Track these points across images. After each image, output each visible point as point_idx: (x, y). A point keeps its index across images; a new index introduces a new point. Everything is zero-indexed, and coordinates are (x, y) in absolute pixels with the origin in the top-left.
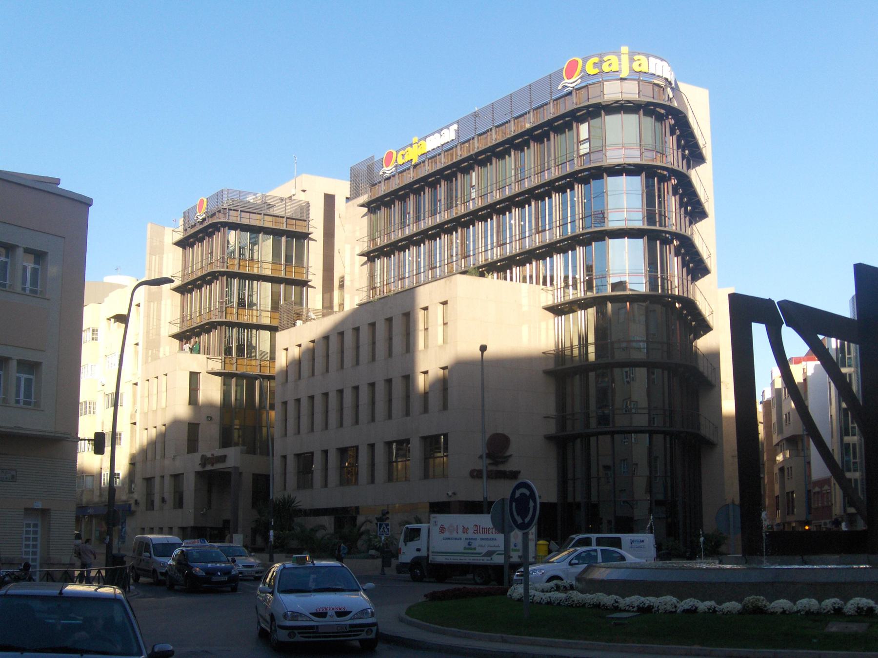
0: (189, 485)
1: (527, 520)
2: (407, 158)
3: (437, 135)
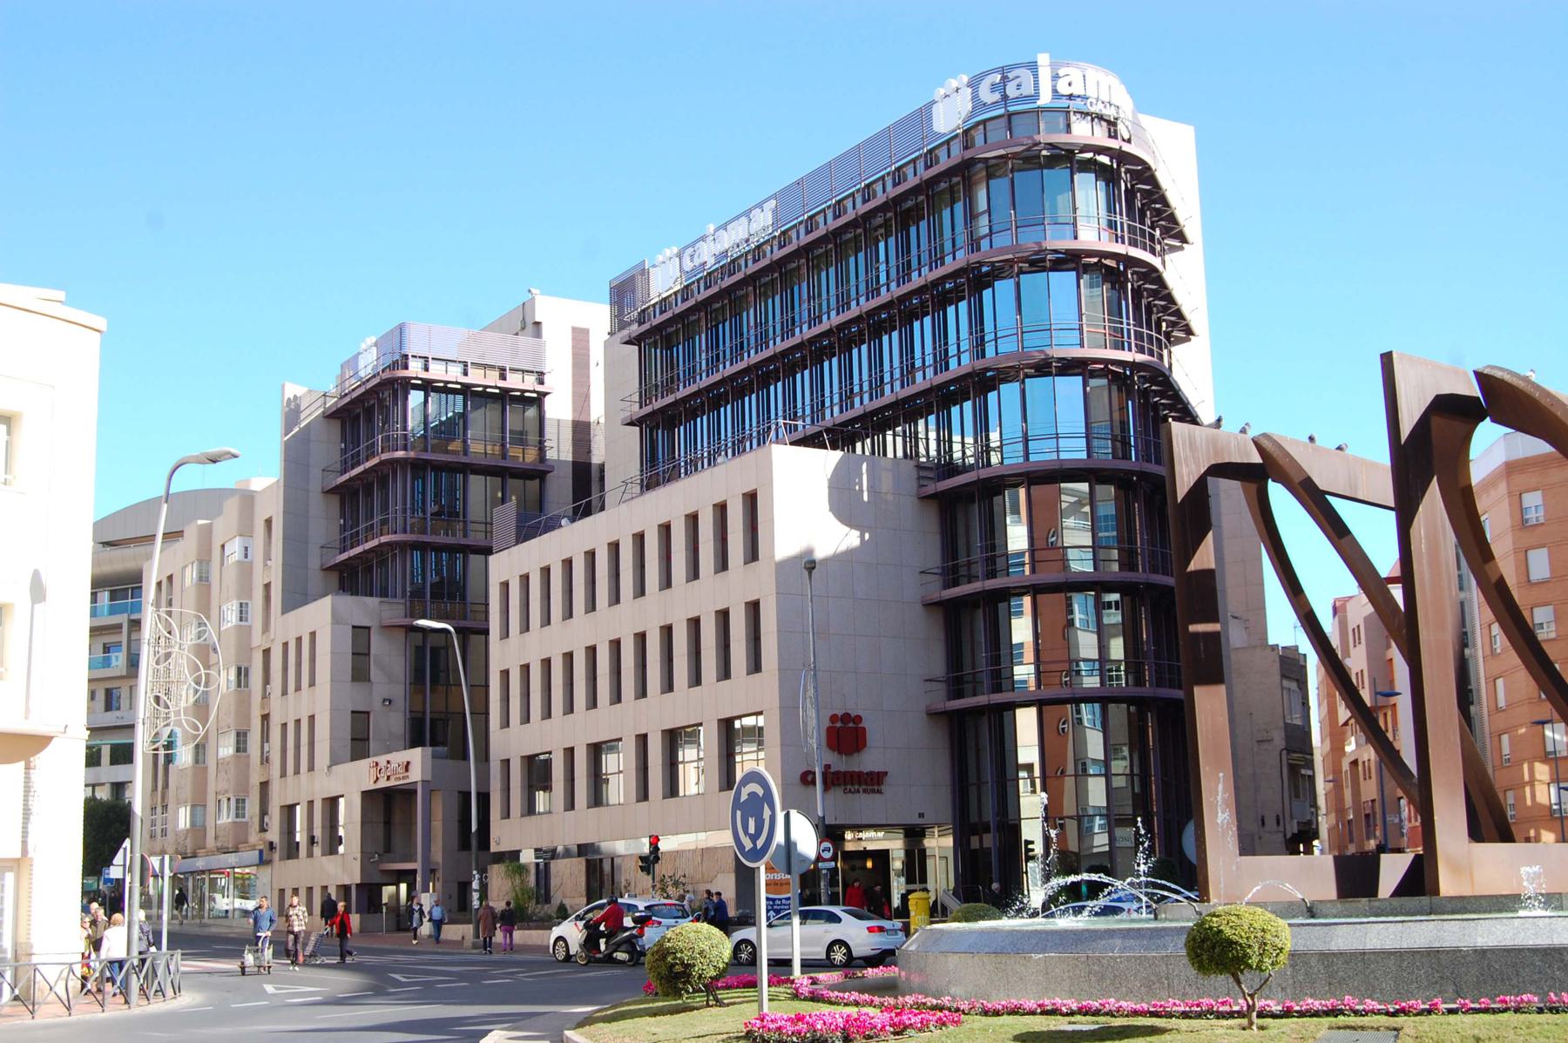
0: (349, 816)
1: (760, 843)
2: (697, 262)
3: (744, 220)
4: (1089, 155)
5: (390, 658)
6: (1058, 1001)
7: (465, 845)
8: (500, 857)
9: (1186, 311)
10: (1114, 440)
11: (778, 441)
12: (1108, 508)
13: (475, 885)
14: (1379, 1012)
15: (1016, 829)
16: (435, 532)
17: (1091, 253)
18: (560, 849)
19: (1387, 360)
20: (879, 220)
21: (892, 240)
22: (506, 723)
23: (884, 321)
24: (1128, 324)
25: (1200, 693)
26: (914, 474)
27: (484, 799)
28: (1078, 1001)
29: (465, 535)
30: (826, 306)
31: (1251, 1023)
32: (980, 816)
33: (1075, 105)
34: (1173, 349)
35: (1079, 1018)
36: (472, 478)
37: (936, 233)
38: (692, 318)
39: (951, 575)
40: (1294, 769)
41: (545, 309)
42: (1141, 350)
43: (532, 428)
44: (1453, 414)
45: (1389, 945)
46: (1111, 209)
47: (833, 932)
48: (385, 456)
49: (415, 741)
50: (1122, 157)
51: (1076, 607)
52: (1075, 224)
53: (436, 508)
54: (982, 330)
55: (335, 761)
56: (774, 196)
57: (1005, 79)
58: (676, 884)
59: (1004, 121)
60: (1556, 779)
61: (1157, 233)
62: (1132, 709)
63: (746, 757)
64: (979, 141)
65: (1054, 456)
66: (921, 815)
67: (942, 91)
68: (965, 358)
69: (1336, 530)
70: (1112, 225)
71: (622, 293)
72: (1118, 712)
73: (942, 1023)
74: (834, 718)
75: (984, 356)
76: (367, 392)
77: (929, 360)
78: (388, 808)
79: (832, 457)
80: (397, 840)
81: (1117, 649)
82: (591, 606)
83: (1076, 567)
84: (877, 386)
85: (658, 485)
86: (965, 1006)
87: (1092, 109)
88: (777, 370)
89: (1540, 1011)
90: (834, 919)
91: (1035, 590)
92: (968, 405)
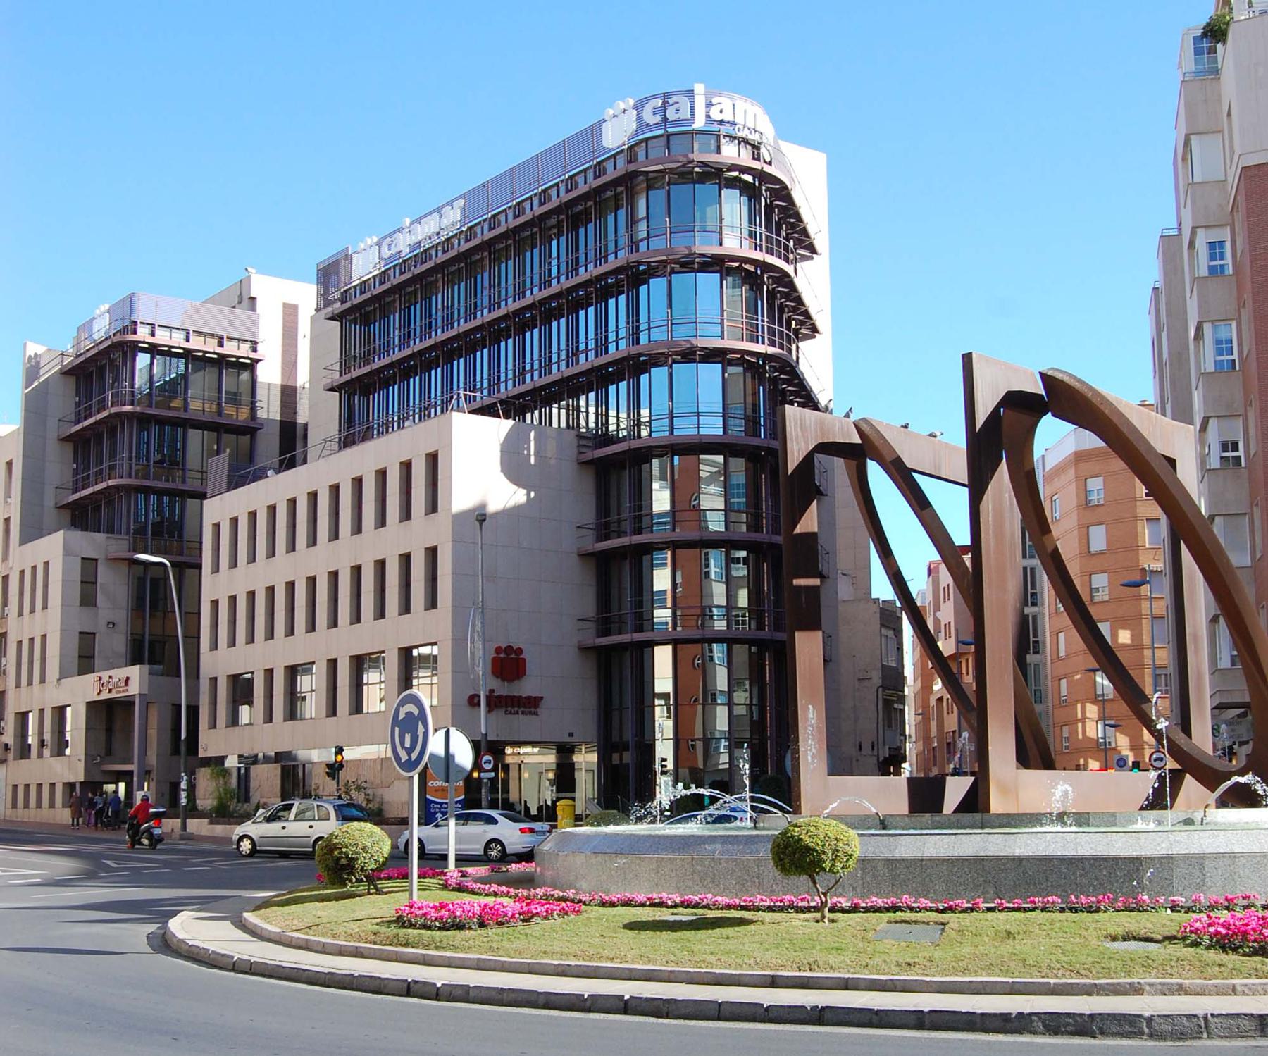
2: (394, 250)
3: (436, 215)
4: (735, 174)
5: (114, 588)
6: (664, 895)
7: (176, 751)
8: (207, 762)
9: (812, 312)
10: (747, 419)
11: (459, 409)
12: (739, 478)
13: (183, 785)
14: (931, 910)
15: (651, 749)
16: (157, 478)
17: (733, 258)
18: (260, 755)
19: (967, 359)
20: (553, 221)
21: (563, 239)
22: (214, 646)
23: (502, 330)
24: (763, 321)
25: (799, 636)
26: (575, 442)
27: (193, 711)
28: (682, 896)
29: (184, 482)
30: (503, 294)
31: (823, 917)
32: (621, 737)
33: (724, 129)
34: (801, 344)
35: (680, 910)
36: (191, 432)
37: (601, 235)
38: (368, 309)
39: (604, 531)
40: (888, 704)
41: (261, 286)
42: (773, 344)
43: (245, 389)
44: (1022, 409)
45: (943, 853)
46: (751, 221)
47: (491, 832)
48: (113, 410)
49: (135, 659)
50: (763, 176)
51: (712, 562)
52: (720, 233)
53: (159, 457)
54: (638, 321)
55: (63, 675)
56: (463, 196)
57: (665, 103)
58: (358, 788)
59: (664, 139)
60: (1103, 717)
61: (791, 244)
62: (754, 649)
63: (421, 681)
64: (641, 156)
65: (695, 432)
66: (571, 735)
67: (611, 112)
68: (623, 344)
69: (919, 503)
70: (752, 235)
71: (328, 275)
72: (741, 651)
73: (564, 913)
74: (498, 650)
75: (638, 343)
76: (99, 353)
77: (591, 345)
78: (109, 717)
79: (503, 426)
80: (116, 745)
81: (743, 599)
82: (357, 529)
83: (713, 527)
84: (546, 365)
85: (354, 443)
86: (586, 898)
87: (739, 134)
88: (460, 348)
89: (1062, 910)
90: (491, 821)
91: (675, 546)
92: (623, 385)
